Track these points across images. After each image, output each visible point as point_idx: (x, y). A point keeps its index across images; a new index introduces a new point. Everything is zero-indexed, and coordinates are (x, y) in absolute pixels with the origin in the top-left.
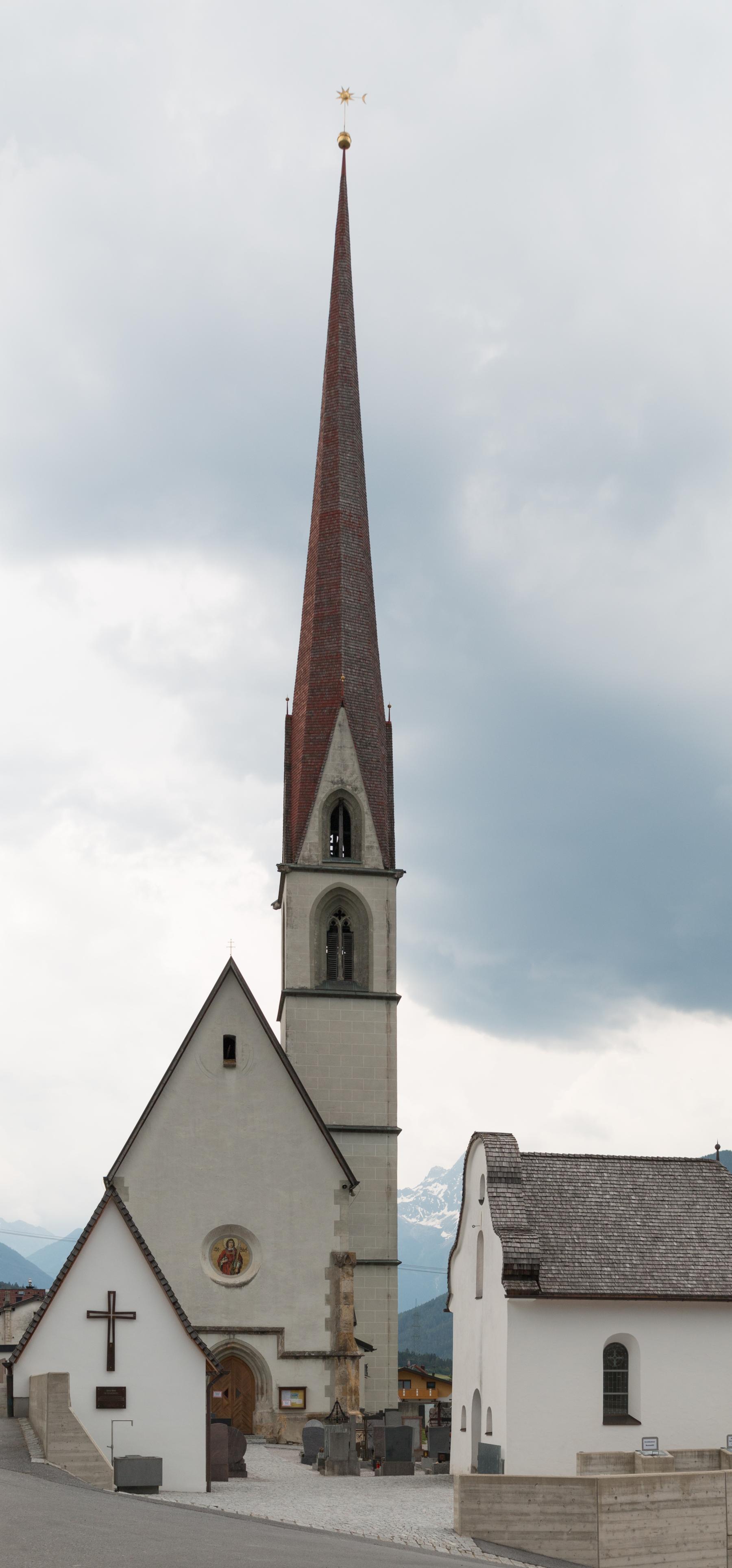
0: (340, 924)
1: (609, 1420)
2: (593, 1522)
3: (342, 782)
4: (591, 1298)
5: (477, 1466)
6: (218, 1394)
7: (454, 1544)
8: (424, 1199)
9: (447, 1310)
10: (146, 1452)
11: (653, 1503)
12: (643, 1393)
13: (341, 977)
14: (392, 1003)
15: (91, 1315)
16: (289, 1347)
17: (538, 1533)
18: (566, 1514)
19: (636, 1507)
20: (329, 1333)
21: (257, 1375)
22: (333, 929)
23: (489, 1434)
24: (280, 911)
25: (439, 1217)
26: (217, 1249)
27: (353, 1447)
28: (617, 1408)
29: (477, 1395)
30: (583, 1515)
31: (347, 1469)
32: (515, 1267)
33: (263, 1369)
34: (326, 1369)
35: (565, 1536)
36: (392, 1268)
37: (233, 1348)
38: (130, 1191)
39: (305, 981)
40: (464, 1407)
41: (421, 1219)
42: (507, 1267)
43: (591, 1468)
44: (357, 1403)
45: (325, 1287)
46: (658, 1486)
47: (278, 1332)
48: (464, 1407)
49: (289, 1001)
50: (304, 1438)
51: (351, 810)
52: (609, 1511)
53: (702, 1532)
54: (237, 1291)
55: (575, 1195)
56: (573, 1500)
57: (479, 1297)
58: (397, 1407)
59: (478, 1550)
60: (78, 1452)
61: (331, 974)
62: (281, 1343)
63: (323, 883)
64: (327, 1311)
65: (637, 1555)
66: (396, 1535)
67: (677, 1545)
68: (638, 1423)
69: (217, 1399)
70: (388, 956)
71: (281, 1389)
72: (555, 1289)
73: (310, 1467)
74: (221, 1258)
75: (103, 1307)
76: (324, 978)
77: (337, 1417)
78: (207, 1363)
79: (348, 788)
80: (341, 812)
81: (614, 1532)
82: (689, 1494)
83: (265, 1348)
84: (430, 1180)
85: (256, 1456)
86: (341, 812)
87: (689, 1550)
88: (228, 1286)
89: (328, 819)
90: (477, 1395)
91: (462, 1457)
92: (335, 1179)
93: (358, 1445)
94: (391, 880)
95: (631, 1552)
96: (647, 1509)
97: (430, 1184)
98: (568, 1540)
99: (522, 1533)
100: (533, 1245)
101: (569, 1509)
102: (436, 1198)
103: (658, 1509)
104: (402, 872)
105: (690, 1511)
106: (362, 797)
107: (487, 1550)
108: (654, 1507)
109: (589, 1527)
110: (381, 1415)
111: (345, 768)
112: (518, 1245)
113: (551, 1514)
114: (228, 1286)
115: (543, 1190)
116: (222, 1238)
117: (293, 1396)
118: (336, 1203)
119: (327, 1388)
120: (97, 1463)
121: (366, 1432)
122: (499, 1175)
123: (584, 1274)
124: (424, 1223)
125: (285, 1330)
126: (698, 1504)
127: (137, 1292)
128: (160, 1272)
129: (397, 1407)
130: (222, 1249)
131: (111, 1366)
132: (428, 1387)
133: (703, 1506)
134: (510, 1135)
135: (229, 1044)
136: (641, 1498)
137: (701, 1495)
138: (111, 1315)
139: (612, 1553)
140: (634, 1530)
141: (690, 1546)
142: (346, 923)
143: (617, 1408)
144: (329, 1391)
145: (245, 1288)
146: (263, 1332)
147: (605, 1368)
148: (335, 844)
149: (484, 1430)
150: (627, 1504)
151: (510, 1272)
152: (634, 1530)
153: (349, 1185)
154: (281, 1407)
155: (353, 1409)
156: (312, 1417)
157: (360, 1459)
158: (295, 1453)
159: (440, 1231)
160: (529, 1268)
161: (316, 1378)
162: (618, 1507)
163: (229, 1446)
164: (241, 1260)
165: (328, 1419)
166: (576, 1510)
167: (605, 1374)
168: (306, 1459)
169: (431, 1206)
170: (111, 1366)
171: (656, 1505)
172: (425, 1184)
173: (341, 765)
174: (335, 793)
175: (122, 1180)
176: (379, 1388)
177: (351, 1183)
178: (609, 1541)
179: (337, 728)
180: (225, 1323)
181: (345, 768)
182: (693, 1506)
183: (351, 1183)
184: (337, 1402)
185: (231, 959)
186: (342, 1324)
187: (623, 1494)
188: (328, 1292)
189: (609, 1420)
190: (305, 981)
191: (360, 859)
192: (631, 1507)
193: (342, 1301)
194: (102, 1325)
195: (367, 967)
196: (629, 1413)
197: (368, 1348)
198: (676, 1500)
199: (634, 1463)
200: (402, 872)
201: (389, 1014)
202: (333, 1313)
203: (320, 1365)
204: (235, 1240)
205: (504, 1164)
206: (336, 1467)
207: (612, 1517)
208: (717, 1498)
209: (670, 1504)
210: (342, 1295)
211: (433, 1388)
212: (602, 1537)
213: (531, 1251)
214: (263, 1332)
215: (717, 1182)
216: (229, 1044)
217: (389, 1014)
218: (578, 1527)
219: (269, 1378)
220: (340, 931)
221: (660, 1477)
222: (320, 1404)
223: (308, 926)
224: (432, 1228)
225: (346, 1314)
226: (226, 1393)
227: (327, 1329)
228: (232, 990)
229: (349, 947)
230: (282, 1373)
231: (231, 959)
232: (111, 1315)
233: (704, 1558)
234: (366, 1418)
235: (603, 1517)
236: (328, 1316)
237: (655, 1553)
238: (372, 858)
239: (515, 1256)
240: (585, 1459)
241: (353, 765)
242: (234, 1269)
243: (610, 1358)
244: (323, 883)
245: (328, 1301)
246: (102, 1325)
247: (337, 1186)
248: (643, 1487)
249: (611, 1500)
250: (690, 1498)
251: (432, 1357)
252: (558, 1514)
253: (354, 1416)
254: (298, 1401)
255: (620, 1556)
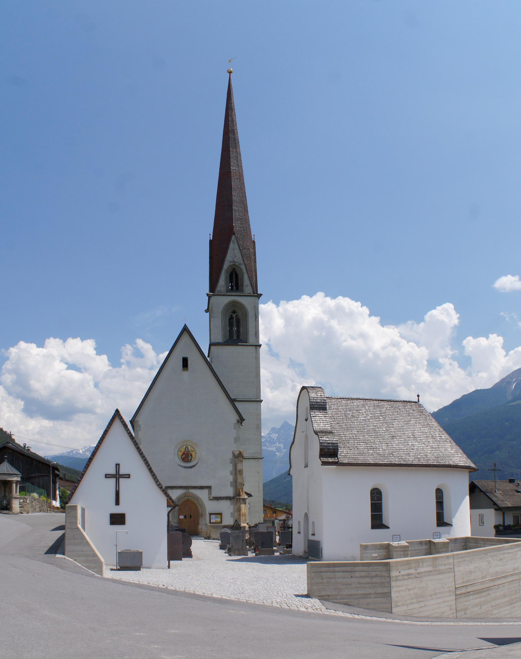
0: (234, 316)
1: (374, 527)
2: (388, 587)
3: (234, 262)
4: (364, 466)
5: (307, 551)
6: (182, 517)
7: (308, 605)
8: (269, 439)
9: (289, 474)
10: (134, 549)
11: (419, 574)
12: (390, 514)
13: (235, 338)
14: (258, 347)
15: (107, 476)
16: (215, 494)
17: (357, 595)
18: (372, 583)
19: (411, 576)
20: (232, 488)
21: (199, 508)
22: (231, 318)
23: (313, 535)
24: (208, 313)
25: (275, 447)
26: (181, 451)
27: (245, 541)
28: (378, 521)
29: (306, 515)
30: (382, 583)
31: (241, 552)
32: (326, 450)
33: (202, 506)
34: (231, 505)
35: (373, 596)
36: (260, 460)
37: (188, 496)
38: (141, 426)
39: (219, 338)
40: (299, 522)
41: (268, 447)
42: (321, 450)
43: (368, 551)
44: (245, 520)
45: (230, 467)
46: (421, 565)
47: (209, 488)
48: (299, 522)
49: (213, 348)
50: (221, 537)
51: (238, 272)
52: (396, 580)
53: (443, 587)
54: (190, 470)
55: (353, 416)
56: (377, 575)
57: (306, 466)
58: (263, 522)
59: (323, 608)
60: (82, 551)
61: (231, 336)
62: (210, 493)
63: (225, 300)
64: (231, 478)
65: (411, 603)
66: (274, 600)
67: (431, 595)
68: (388, 528)
69: (181, 519)
70: (256, 328)
71: (210, 514)
72: (346, 461)
73: (224, 551)
74: (182, 455)
75: (113, 472)
76: (228, 338)
77: (236, 527)
78: (167, 500)
79: (237, 264)
80: (234, 273)
81: (399, 591)
82: (436, 567)
83: (203, 495)
84: (271, 432)
85: (198, 545)
86: (234, 273)
87: (437, 598)
88: (185, 467)
89: (228, 276)
90: (306, 515)
91: (299, 545)
92: (234, 417)
93: (247, 540)
94: (256, 298)
95: (409, 602)
96: (416, 577)
97: (271, 434)
98: (374, 598)
99: (348, 595)
100: (335, 439)
101: (374, 580)
102: (273, 439)
103: (421, 577)
104: (261, 295)
105: (437, 577)
106: (243, 267)
107: (329, 607)
108: (419, 576)
109: (386, 590)
110: (256, 526)
111: (236, 257)
112: (327, 439)
113: (364, 584)
114: (185, 467)
115: (337, 414)
116: (183, 446)
117: (216, 517)
118: (235, 429)
119: (231, 514)
120: (94, 558)
121: (250, 534)
122: (316, 406)
123: (361, 454)
124: (269, 449)
125: (212, 488)
126: (441, 573)
127: (132, 464)
128: (142, 453)
129: (263, 522)
130: (183, 450)
131: (117, 503)
132: (273, 513)
133: (444, 573)
134: (320, 387)
135: (185, 363)
136: (412, 571)
137: (442, 568)
138: (117, 476)
139: (399, 604)
140: (409, 590)
141: (438, 596)
142: (237, 315)
143: (378, 521)
144: (232, 515)
145: (193, 469)
146: (202, 488)
147: (371, 501)
148: (232, 286)
149: (310, 533)
150: (405, 575)
151: (323, 453)
152: (409, 590)
153: (240, 421)
154: (210, 523)
155: (244, 523)
156: (225, 527)
157: (248, 547)
158: (218, 543)
159: (276, 452)
160: (333, 451)
161: (226, 509)
162: (401, 578)
163: (183, 543)
164: (191, 455)
165: (232, 527)
166: (378, 580)
167: (371, 504)
168: (222, 547)
169: (272, 442)
170: (117, 503)
171: (420, 575)
172: (269, 434)
173: (233, 254)
174: (231, 266)
175: (138, 421)
176: (252, 515)
177: (241, 420)
178: (397, 597)
179: (231, 242)
180: (184, 484)
181: (236, 257)
182: (439, 574)
183: (241, 420)
184: (236, 520)
185: (185, 325)
186: (238, 484)
187: (404, 570)
188: (231, 469)
189: (374, 527)
190: (219, 338)
191: (243, 290)
192: (407, 577)
193: (238, 473)
194: (113, 480)
195: (246, 333)
196: (384, 523)
197: (249, 495)
198: (430, 571)
199: (389, 548)
200: (261, 295)
201: (256, 352)
202: (234, 479)
203: (227, 503)
204: (189, 447)
205: (318, 401)
206: (236, 552)
207: (398, 583)
208: (450, 569)
209: (427, 573)
210: (238, 471)
211: (276, 513)
212: (393, 595)
213: (334, 442)
214: (202, 488)
215: (419, 412)
216: (185, 363)
217: (256, 352)
218: (380, 590)
219: (205, 509)
220: (234, 319)
221: (421, 559)
222: (228, 521)
223: (220, 317)
224: (272, 451)
225: (239, 480)
226: (185, 517)
227: (231, 486)
228: (186, 338)
229: (238, 326)
230: (210, 506)
231: (185, 325)
232: (117, 476)
233: (444, 602)
234: (250, 527)
235: (393, 584)
236: (232, 480)
237: (421, 602)
238: (248, 289)
239: (326, 444)
240: (364, 548)
241: (239, 255)
242: (188, 460)
243: (373, 495)
244: (225, 300)
245: (231, 473)
246: (113, 480)
247: (235, 422)
248: (413, 565)
249: (397, 574)
250: (437, 569)
251: (273, 501)
252: (368, 583)
253: (244, 527)
254: (219, 520)
255: (403, 605)
